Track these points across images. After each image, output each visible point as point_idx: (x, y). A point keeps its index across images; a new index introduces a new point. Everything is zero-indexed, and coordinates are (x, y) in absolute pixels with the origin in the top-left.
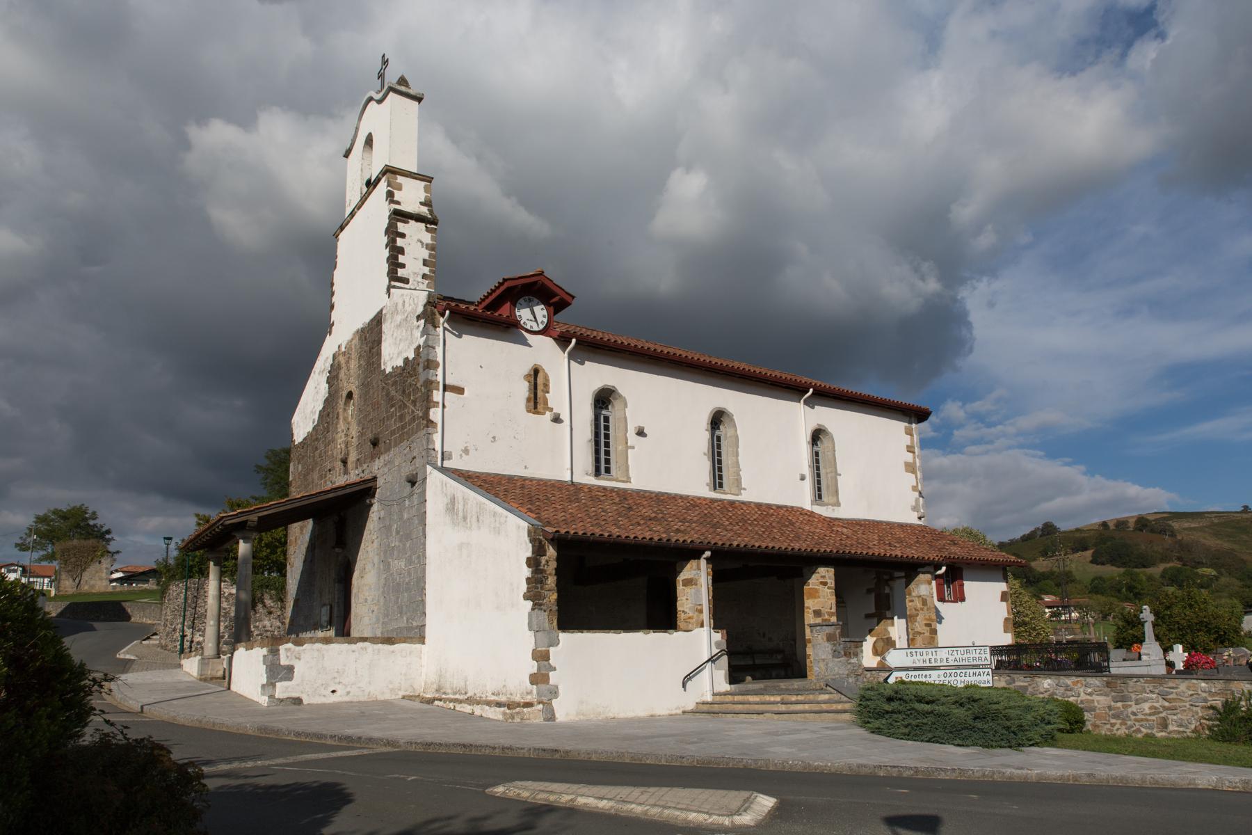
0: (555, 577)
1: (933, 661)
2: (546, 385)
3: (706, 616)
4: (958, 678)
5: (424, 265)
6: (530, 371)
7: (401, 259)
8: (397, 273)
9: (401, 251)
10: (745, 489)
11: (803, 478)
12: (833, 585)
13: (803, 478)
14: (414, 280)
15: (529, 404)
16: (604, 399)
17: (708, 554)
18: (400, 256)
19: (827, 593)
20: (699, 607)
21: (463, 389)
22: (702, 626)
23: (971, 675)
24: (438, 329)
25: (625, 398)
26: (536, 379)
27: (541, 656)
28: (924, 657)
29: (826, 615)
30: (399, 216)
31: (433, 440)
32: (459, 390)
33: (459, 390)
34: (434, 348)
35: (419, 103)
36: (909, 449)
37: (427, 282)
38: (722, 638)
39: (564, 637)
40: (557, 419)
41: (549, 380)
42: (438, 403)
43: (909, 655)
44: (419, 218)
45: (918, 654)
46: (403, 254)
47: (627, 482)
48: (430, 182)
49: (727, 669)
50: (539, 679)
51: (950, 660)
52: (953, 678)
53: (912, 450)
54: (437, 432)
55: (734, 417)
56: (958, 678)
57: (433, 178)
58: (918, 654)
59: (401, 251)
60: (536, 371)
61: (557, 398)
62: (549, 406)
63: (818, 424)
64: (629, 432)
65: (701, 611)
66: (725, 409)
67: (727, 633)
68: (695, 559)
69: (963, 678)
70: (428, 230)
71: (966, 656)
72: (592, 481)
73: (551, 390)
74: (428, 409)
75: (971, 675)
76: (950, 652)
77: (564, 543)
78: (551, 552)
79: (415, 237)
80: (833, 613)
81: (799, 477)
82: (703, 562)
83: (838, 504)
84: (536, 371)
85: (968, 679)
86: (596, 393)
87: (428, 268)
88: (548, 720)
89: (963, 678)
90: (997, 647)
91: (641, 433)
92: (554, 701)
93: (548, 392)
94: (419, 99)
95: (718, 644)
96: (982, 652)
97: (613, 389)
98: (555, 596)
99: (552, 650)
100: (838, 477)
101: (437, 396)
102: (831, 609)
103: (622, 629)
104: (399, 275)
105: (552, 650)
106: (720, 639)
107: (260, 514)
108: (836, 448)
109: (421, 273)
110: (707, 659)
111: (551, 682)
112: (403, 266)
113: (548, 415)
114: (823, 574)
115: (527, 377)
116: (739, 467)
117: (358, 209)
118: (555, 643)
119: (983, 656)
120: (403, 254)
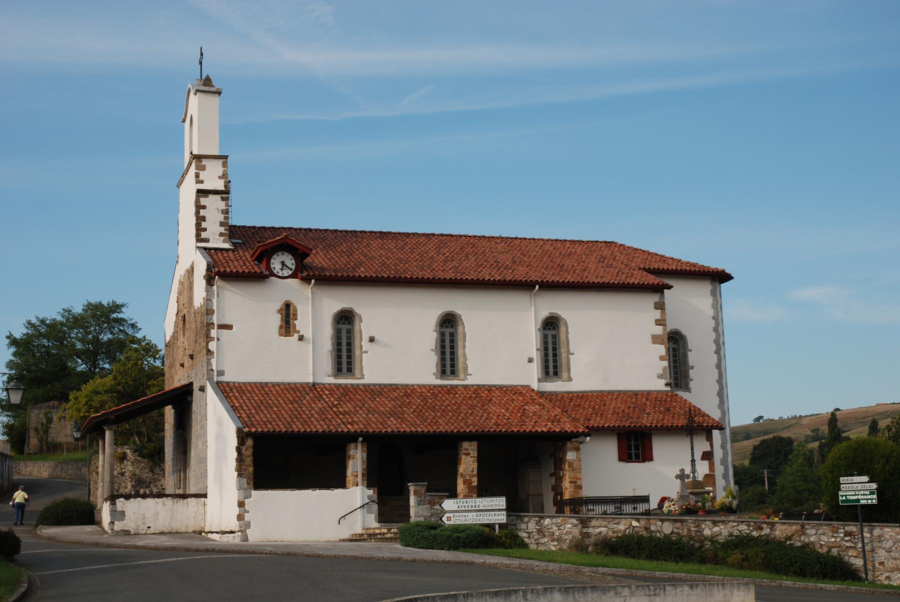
0: (252, 458)
1: (470, 506)
2: (295, 315)
3: (360, 479)
4: (485, 517)
5: (221, 226)
6: (282, 306)
7: (204, 225)
8: (201, 236)
9: (204, 219)
10: (470, 375)
11: (530, 360)
12: (476, 455)
13: (530, 360)
14: (214, 239)
15: (282, 330)
16: (345, 318)
17: (361, 439)
18: (203, 223)
19: (470, 460)
20: (355, 474)
21: (232, 326)
22: (357, 485)
23: (493, 515)
24: (213, 287)
25: (360, 315)
26: (288, 313)
27: (241, 504)
28: (465, 504)
29: (467, 476)
30: (202, 193)
31: (211, 364)
32: (229, 327)
33: (229, 327)
34: (211, 301)
35: (219, 96)
36: (658, 323)
37: (223, 238)
38: (373, 493)
39: (254, 493)
40: (301, 338)
41: (297, 311)
42: (214, 338)
43: (455, 502)
44: (216, 192)
45: (461, 502)
46: (205, 221)
47: (361, 378)
48: (227, 159)
49: (377, 513)
50: (240, 517)
51: (480, 506)
52: (482, 517)
53: (662, 322)
54: (214, 358)
55: (462, 317)
56: (485, 517)
57: (228, 156)
58: (486, 501)
59: (204, 219)
60: (288, 305)
61: (303, 322)
62: (297, 329)
63: (550, 313)
64: (363, 341)
65: (357, 476)
66: (453, 311)
67: (378, 489)
68: (353, 442)
69: (488, 518)
70: (223, 199)
71: (490, 503)
72: (332, 380)
73: (298, 318)
74: (208, 343)
75: (493, 515)
76: (481, 501)
77: (257, 437)
78: (250, 442)
79: (213, 204)
80: (474, 475)
81: (527, 360)
82: (359, 445)
83: (570, 379)
84: (288, 305)
85: (490, 518)
86: (335, 315)
87: (224, 228)
88: (244, 541)
89: (488, 518)
90: (639, 496)
91: (372, 340)
92: (247, 530)
93: (296, 319)
94: (219, 93)
95: (369, 497)
96: (501, 501)
97: (351, 310)
98: (251, 469)
99: (246, 501)
100: (571, 356)
101: (214, 333)
102: (472, 472)
103: (295, 488)
104: (202, 237)
105: (246, 501)
106: (372, 494)
107: (116, 414)
108: (569, 332)
109: (219, 232)
110: (359, 506)
111: (246, 520)
112: (205, 230)
113: (296, 336)
114: (466, 448)
115: (280, 311)
116: (466, 357)
117: (186, 175)
118: (249, 496)
119: (501, 504)
120: (205, 221)
